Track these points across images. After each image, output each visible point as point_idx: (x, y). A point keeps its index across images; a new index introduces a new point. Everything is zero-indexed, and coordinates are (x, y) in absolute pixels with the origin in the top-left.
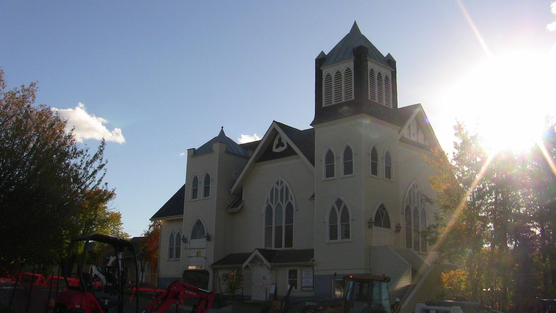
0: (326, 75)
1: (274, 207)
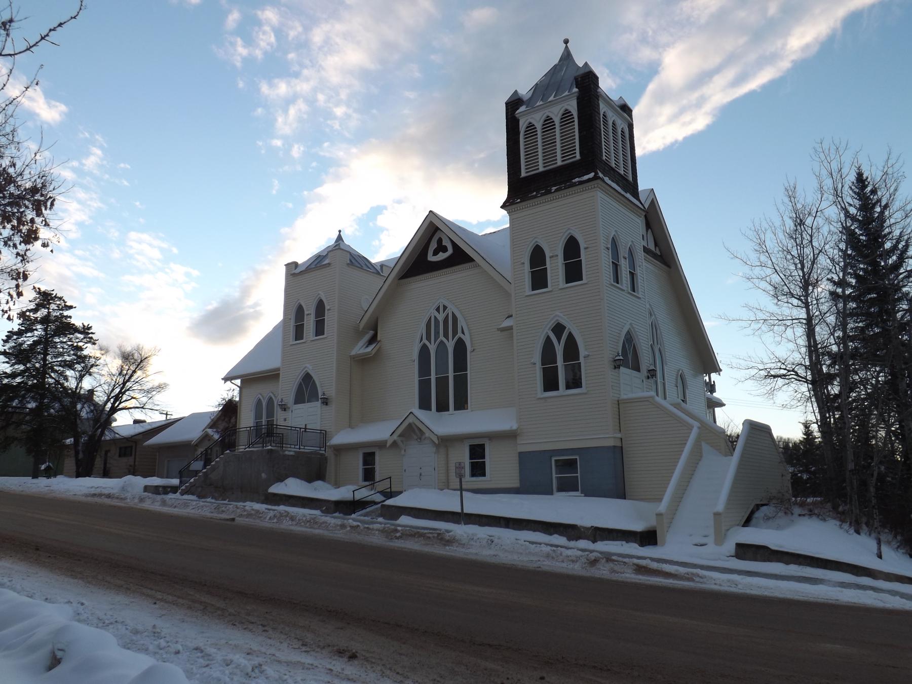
0: (525, 126)
1: (432, 348)
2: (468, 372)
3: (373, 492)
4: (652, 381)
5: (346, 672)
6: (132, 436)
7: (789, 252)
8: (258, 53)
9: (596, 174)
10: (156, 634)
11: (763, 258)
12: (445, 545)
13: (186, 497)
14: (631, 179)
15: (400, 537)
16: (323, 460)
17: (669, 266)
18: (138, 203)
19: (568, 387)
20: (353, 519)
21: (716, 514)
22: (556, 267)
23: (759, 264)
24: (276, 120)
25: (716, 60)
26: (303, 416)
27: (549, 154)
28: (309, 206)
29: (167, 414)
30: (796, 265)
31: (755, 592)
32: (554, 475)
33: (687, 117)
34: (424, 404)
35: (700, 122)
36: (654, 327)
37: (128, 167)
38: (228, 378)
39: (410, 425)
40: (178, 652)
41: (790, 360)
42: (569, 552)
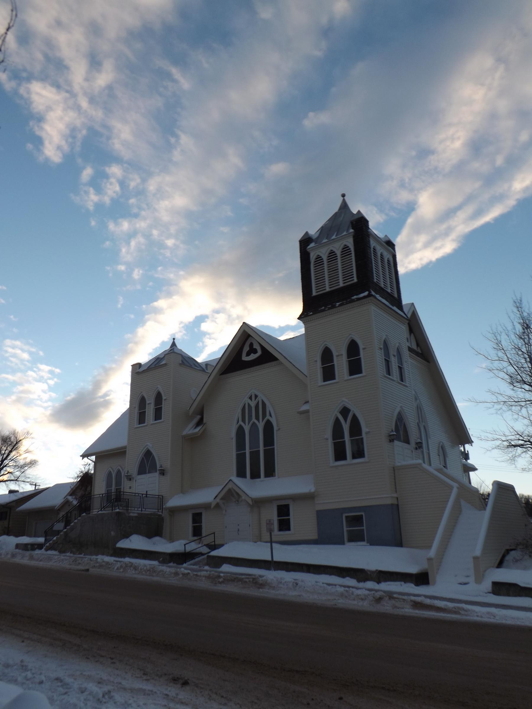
0: (315, 257)
1: (247, 428)
2: (275, 447)
3: (200, 545)
4: (419, 451)
5: (180, 697)
6: (7, 504)
7: (520, 349)
8: (107, 200)
9: (370, 292)
10: (24, 667)
11: (500, 354)
12: (259, 588)
13: (49, 552)
14: (396, 295)
15: (223, 582)
16: (161, 519)
17: (428, 362)
18: (12, 317)
19: (354, 457)
20: (185, 568)
21: (476, 558)
22: (341, 364)
23: (497, 358)
24: (120, 250)
25: (459, 199)
26: (146, 484)
27: (333, 277)
28: (147, 316)
29: (36, 485)
30: (525, 358)
31: (509, 622)
32: (345, 529)
33: (438, 244)
34: (241, 474)
35: (448, 247)
36: (419, 409)
37: (5, 288)
38: (85, 455)
39: (230, 491)
40: (41, 682)
41: (526, 433)
42: (359, 592)
